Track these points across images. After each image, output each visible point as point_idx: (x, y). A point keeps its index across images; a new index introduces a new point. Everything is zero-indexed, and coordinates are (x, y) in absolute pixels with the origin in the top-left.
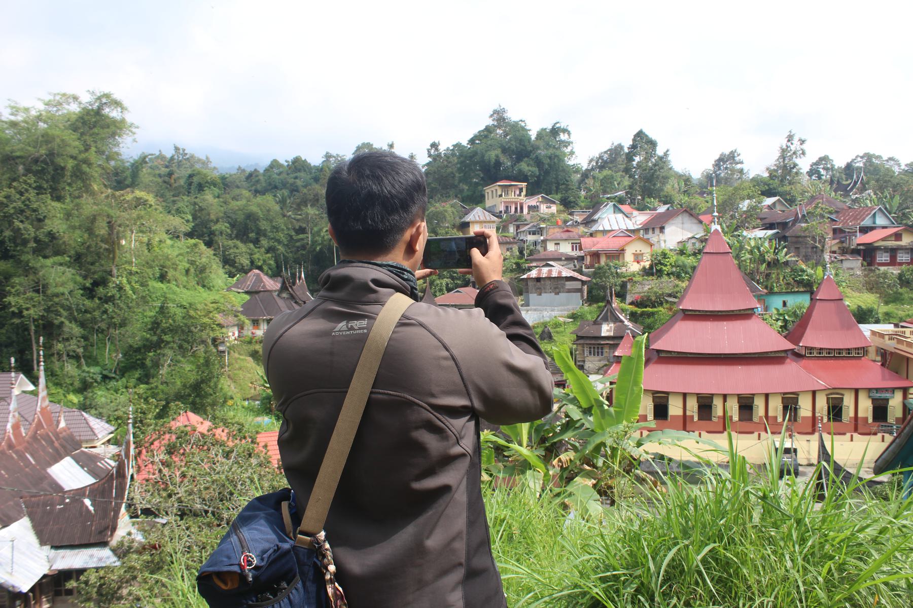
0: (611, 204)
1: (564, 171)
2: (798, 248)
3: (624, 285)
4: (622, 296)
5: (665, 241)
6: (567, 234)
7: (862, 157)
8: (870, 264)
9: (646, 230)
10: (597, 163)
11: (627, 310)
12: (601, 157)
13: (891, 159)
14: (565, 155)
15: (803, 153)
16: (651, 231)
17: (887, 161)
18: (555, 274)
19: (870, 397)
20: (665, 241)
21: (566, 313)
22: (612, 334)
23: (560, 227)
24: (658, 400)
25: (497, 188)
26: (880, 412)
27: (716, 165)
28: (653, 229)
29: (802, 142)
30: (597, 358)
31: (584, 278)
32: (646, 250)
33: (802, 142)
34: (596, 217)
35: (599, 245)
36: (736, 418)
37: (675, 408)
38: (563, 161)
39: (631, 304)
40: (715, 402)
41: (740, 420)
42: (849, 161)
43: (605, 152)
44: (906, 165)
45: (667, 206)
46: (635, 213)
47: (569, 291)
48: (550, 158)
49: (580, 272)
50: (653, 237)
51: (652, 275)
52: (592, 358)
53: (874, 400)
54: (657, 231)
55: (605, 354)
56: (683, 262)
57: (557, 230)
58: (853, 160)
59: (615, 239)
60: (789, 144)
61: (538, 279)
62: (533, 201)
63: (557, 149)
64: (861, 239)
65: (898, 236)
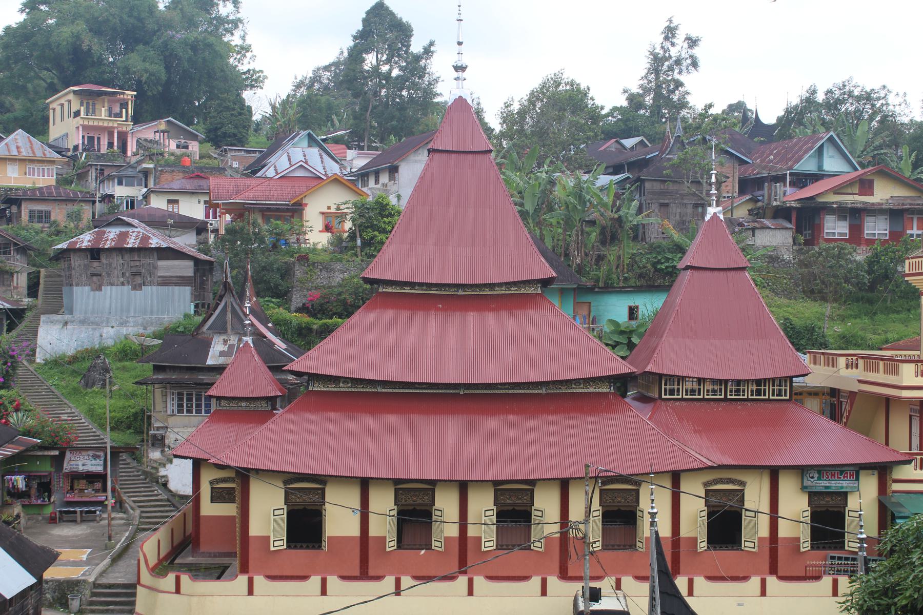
2: (666, 205)
3: (286, 272)
6: (197, 182)
8: (809, 243)
12: (316, 78)
15: (695, 64)
18: (132, 242)
19: (803, 488)
21: (151, 330)
24: (299, 499)
25: (71, 97)
26: (828, 523)
28: (377, 174)
29: (693, 42)
33: (693, 42)
36: (489, 543)
37: (340, 519)
40: (439, 503)
41: (500, 547)
43: (326, 68)
47: (166, 282)
52: (184, 419)
53: (813, 496)
54: (384, 178)
59: (284, 183)
60: (667, 45)
61: (95, 253)
62: (148, 132)
64: (789, 195)
65: (866, 186)
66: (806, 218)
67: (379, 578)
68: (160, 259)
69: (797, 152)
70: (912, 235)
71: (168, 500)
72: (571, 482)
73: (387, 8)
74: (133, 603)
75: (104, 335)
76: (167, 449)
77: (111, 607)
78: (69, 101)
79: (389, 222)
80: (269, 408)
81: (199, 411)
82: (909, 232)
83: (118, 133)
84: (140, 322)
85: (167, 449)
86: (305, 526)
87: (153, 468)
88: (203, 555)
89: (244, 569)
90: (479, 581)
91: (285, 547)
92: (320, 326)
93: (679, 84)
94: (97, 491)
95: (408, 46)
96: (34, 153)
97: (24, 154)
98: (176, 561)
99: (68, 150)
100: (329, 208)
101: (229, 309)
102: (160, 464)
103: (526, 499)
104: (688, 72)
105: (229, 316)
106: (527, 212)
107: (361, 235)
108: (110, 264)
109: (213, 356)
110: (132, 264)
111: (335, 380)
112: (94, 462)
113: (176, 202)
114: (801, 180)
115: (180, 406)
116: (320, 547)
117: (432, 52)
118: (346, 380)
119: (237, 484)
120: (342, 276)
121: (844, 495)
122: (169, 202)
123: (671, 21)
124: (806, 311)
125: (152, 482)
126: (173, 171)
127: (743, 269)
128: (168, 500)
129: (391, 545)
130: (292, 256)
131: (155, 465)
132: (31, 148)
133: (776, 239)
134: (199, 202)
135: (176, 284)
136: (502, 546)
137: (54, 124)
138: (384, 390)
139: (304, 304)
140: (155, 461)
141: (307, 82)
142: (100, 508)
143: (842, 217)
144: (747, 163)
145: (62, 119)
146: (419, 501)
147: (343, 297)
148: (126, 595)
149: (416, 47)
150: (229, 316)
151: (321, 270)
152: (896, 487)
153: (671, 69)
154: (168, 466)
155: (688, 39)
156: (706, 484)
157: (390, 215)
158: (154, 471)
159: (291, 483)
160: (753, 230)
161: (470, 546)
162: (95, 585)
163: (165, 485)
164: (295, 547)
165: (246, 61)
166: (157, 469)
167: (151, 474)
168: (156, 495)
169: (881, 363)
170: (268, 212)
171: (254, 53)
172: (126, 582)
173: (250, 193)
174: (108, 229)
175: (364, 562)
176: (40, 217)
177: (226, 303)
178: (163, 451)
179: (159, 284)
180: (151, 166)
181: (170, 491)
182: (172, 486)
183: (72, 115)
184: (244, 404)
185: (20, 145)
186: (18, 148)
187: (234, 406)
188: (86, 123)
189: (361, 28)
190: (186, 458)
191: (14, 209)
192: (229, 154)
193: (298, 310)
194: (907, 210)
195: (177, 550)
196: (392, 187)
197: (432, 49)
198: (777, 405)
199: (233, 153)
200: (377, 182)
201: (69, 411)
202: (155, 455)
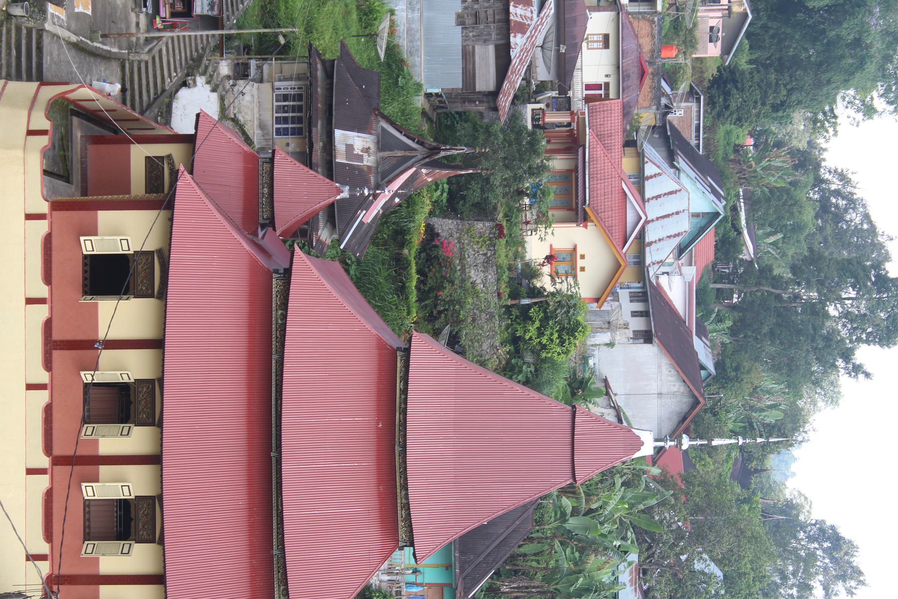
0: (720, 207)
1: (818, 85)
3: (483, 211)
4: (454, 203)
5: (611, 345)
6: (634, 71)
9: (641, 296)
10: (837, 193)
11: (411, 217)
12: (852, 202)
14: (864, 90)
16: (638, 307)
20: (611, 345)
21: (403, 42)
22: (340, 159)
23: (655, 53)
24: (140, 267)
27: (822, 530)
28: (645, 314)
30: (269, 117)
31: (505, 102)
32: (586, 285)
34: (681, 163)
35: (599, 151)
36: (91, 491)
37: (121, 315)
38: (846, 83)
39: (430, 230)
41: (87, 504)
43: (867, 217)
45: (710, 365)
46: (691, 272)
47: (468, 56)
48: (857, 42)
49: (523, 96)
50: (625, 307)
51: (514, 295)
54: (638, 324)
55: (280, 141)
56: (549, 383)
57: (647, 44)
59: (617, 196)
63: (882, 68)
67: (48, 365)
68: (497, 48)
71: (163, 91)
72: (162, 586)
74: (19, 78)
76: (231, 82)
77: (14, 52)
79: (552, 340)
80: (261, 221)
81: (278, 120)
84: (413, 26)
85: (231, 82)
86: (109, 276)
87: (207, 67)
88: (84, 149)
89: (56, 206)
91: (85, 253)
92: (406, 259)
94: (172, 6)
95: (867, 342)
98: (75, 120)
100: (583, 257)
101: (408, 154)
102: (211, 76)
103: (144, 534)
105: (400, 153)
106: (565, 521)
107: (535, 304)
109: (346, 137)
110: (490, 12)
111: (284, 305)
113: (606, 45)
115: (285, 98)
116: (85, 293)
117: (856, 376)
118: (285, 317)
119: (160, 194)
120: (479, 281)
122: (606, 37)
125: (188, 68)
126: (653, 36)
128: (163, 91)
130: (506, 215)
131: (210, 69)
134: (607, 76)
135: (465, 70)
136: (89, 506)
138: (274, 362)
139: (438, 235)
140: (216, 69)
142: (150, 12)
146: (141, 407)
147: (447, 285)
148: (29, 68)
150: (400, 153)
151: (485, 254)
154: (208, 87)
157: (562, 343)
158: (201, 69)
159: (159, 258)
161: (89, 469)
162: (41, 32)
163: (185, 84)
164: (85, 265)
165: (851, 112)
166: (204, 74)
167: (199, 66)
168: (170, 76)
170: (571, 180)
171: (861, 124)
172: (45, 66)
175: (66, 345)
177: (415, 150)
180: (659, 8)
181: (177, 91)
182: (183, 93)
184: (266, 190)
187: (263, 180)
190: (196, 128)
192: (694, 105)
193: (430, 229)
195: (91, 116)
196: (621, 336)
197: (861, 376)
199: (695, 109)
200: (634, 314)
202: (225, 68)
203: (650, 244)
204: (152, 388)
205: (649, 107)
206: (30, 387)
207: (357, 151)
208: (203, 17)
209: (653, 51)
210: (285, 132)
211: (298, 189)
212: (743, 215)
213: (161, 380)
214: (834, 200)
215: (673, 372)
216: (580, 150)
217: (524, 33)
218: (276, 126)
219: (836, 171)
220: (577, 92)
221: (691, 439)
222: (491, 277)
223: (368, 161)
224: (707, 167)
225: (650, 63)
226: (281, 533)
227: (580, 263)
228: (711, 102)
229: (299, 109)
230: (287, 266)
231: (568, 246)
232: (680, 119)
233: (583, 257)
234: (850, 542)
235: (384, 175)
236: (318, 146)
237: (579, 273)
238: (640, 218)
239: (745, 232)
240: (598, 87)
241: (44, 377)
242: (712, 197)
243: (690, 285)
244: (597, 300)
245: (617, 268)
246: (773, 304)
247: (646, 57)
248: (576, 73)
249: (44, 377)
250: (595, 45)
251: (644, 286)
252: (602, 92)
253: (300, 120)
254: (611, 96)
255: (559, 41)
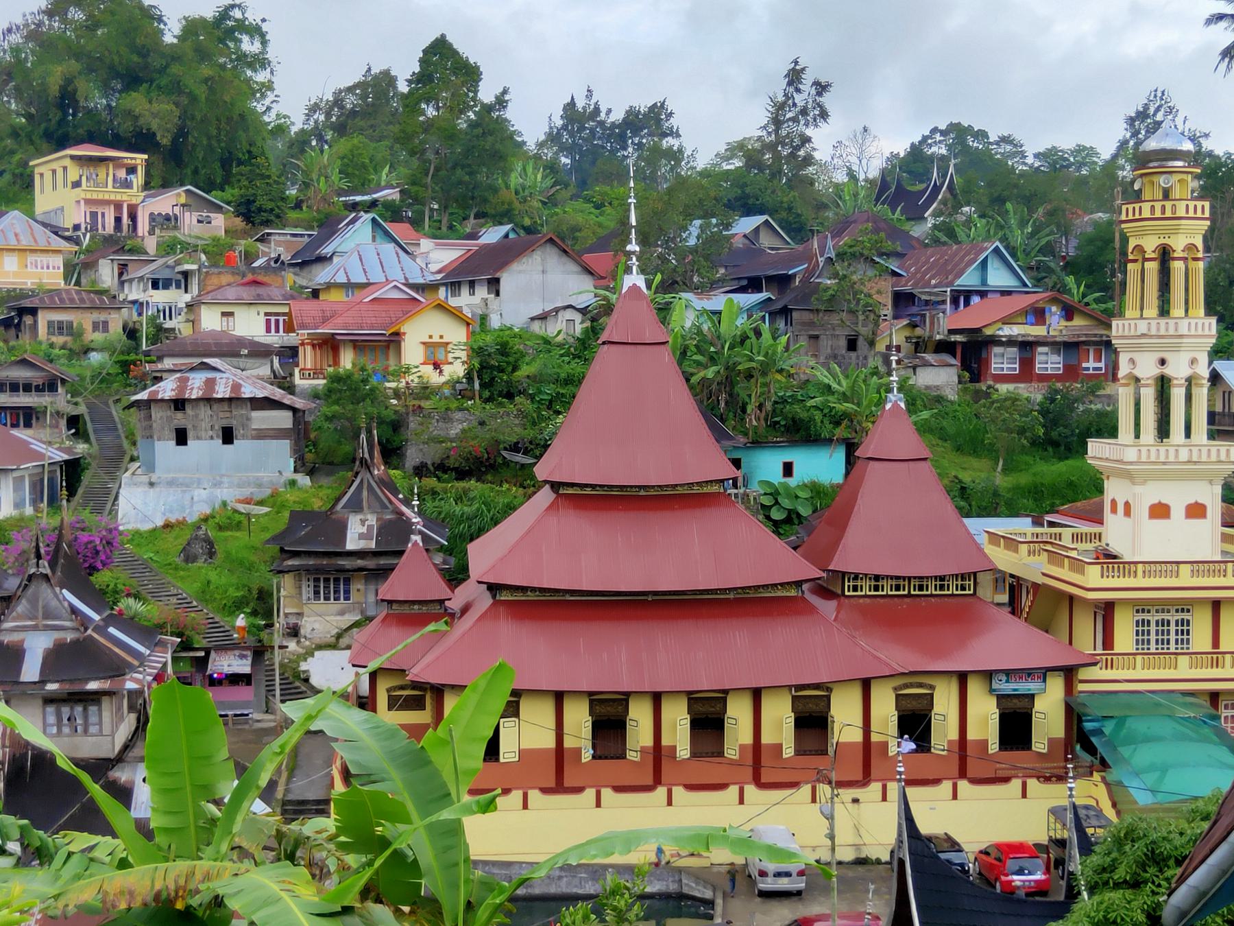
6: (255, 290)
7: (943, 133)
8: (976, 378)
9: (455, 287)
10: (328, 115)
13: (1005, 140)
15: (824, 115)
16: (465, 291)
17: (997, 143)
18: (222, 391)
19: (991, 691)
22: (372, 545)
25: (67, 162)
28: (472, 284)
29: (821, 88)
34: (327, 250)
36: (684, 752)
42: (917, 139)
43: (350, 90)
44: (1037, 156)
46: (426, 244)
47: (262, 435)
53: (1001, 698)
55: (354, 596)
58: (925, 138)
59: (376, 307)
66: (971, 352)
67: (579, 790)
68: (253, 409)
69: (956, 265)
70: (1088, 369)
73: (451, 45)
75: (196, 499)
78: (65, 168)
82: (1084, 365)
83: (129, 206)
90: (678, 791)
93: (806, 140)
95: (476, 92)
96: (36, 241)
97: (24, 242)
99: (68, 230)
101: (365, 486)
103: (718, 707)
104: (816, 126)
105: (365, 493)
108: (197, 416)
110: (221, 415)
112: (240, 662)
114: (962, 297)
115: (317, 593)
117: (507, 102)
118: (533, 589)
121: (1031, 697)
123: (796, 63)
124: (975, 472)
126: (220, 273)
127: (925, 459)
129: (587, 755)
132: (32, 234)
133: (941, 377)
137: (42, 191)
141: (323, 105)
143: (1013, 351)
144: (900, 275)
145: (54, 187)
149: (487, 94)
150: (365, 493)
152: (1081, 687)
153: (795, 120)
154: (310, 659)
155: (817, 83)
156: (895, 689)
160: (914, 368)
163: (306, 680)
169: (1066, 560)
173: (340, 320)
174: (191, 375)
176: (59, 328)
178: (298, 642)
179: (254, 438)
180: (195, 267)
183: (70, 185)
184: (416, 607)
185: (18, 231)
186: (16, 235)
187: (406, 609)
188: (89, 196)
189: (417, 70)
191: (28, 320)
192: (272, 238)
194: (1083, 343)
197: (507, 97)
198: (960, 599)
199: (277, 237)
201: (175, 592)
203: (406, 279)
204: (596, 700)
205: (283, 277)
206: (598, 805)
207: (364, 530)
208: (254, 664)
209: (233, 274)
210: (347, 592)
211: (415, 576)
212: (358, 198)
213: (590, 694)
214: (334, 119)
215: (524, 260)
216: (339, 337)
217: (240, 385)
218: (342, 600)
219: (307, 115)
220: (276, 339)
221: (630, 243)
222: (458, 415)
223: (372, 520)
224: (328, 226)
225: (244, 276)
226: (695, 592)
227: (436, 339)
228: (267, 223)
229: (327, 580)
230: (485, 586)
231: (422, 347)
232: (287, 249)
233: (431, 337)
234: (627, 112)
235: (384, 507)
236: (360, 563)
237: (445, 340)
238: (395, 287)
239: (375, 196)
240: (268, 322)
241: (590, 793)
242: (358, 224)
243: (437, 244)
244: (468, 324)
245: (442, 307)
246: (443, 173)
247: (238, 278)
248: (256, 339)
249: (590, 793)
250: (231, 324)
251: (445, 284)
252: (273, 319)
253: (337, 580)
254: (287, 310)
255: (237, 355)
